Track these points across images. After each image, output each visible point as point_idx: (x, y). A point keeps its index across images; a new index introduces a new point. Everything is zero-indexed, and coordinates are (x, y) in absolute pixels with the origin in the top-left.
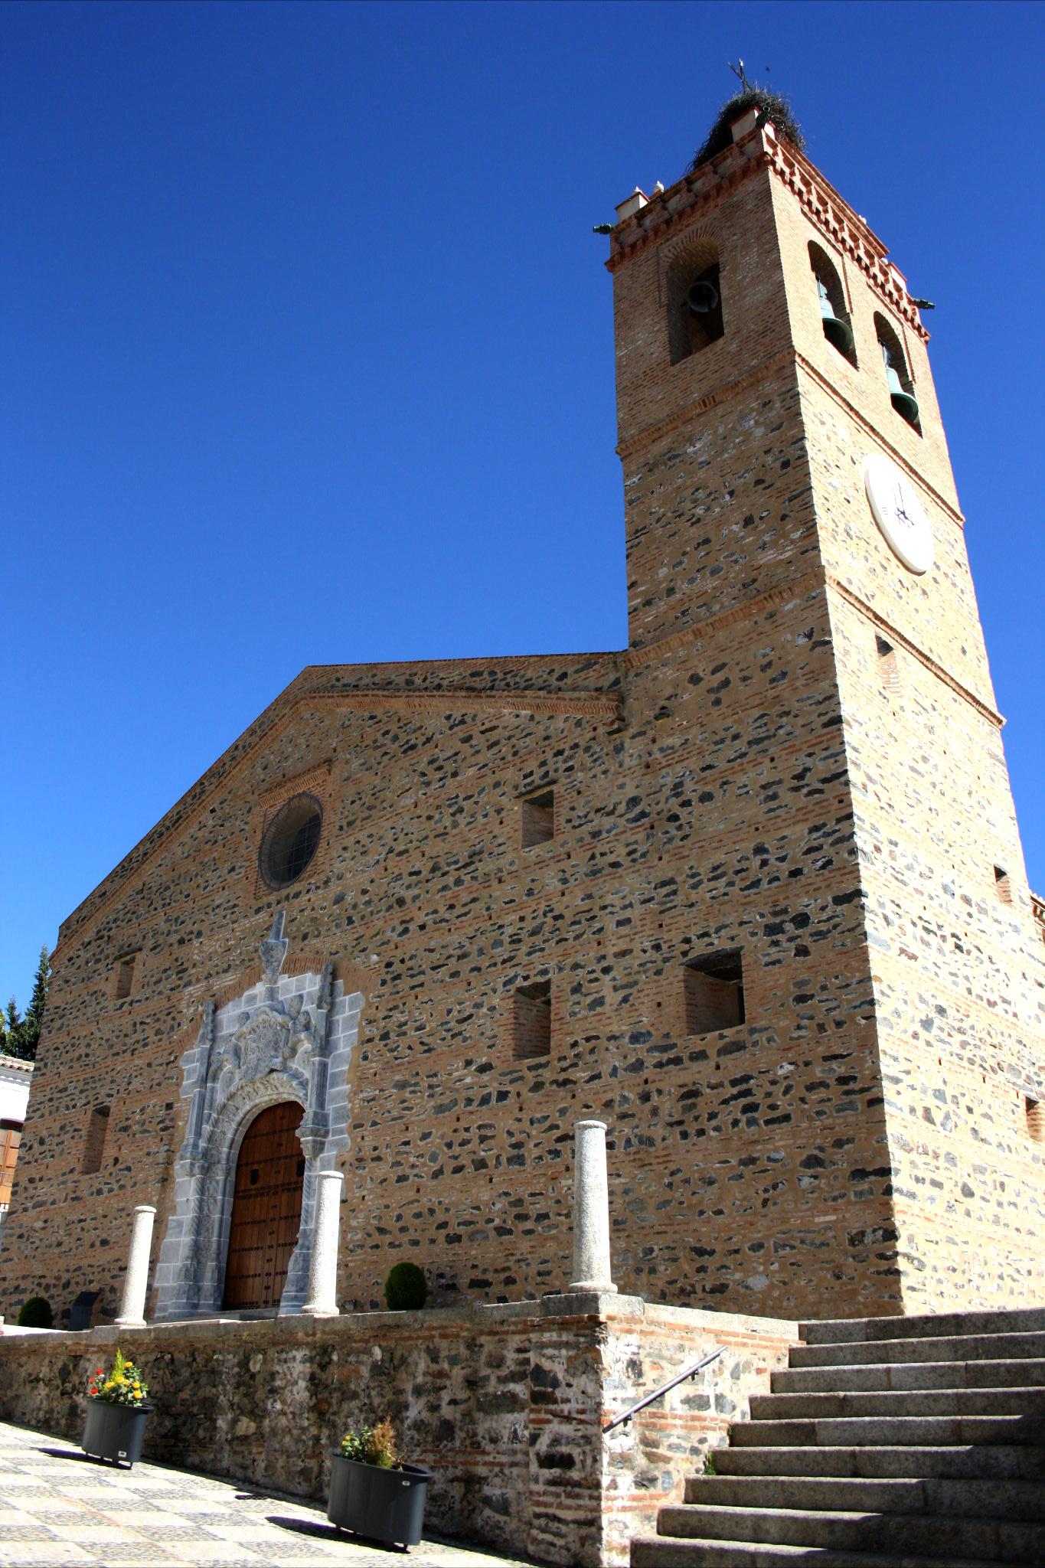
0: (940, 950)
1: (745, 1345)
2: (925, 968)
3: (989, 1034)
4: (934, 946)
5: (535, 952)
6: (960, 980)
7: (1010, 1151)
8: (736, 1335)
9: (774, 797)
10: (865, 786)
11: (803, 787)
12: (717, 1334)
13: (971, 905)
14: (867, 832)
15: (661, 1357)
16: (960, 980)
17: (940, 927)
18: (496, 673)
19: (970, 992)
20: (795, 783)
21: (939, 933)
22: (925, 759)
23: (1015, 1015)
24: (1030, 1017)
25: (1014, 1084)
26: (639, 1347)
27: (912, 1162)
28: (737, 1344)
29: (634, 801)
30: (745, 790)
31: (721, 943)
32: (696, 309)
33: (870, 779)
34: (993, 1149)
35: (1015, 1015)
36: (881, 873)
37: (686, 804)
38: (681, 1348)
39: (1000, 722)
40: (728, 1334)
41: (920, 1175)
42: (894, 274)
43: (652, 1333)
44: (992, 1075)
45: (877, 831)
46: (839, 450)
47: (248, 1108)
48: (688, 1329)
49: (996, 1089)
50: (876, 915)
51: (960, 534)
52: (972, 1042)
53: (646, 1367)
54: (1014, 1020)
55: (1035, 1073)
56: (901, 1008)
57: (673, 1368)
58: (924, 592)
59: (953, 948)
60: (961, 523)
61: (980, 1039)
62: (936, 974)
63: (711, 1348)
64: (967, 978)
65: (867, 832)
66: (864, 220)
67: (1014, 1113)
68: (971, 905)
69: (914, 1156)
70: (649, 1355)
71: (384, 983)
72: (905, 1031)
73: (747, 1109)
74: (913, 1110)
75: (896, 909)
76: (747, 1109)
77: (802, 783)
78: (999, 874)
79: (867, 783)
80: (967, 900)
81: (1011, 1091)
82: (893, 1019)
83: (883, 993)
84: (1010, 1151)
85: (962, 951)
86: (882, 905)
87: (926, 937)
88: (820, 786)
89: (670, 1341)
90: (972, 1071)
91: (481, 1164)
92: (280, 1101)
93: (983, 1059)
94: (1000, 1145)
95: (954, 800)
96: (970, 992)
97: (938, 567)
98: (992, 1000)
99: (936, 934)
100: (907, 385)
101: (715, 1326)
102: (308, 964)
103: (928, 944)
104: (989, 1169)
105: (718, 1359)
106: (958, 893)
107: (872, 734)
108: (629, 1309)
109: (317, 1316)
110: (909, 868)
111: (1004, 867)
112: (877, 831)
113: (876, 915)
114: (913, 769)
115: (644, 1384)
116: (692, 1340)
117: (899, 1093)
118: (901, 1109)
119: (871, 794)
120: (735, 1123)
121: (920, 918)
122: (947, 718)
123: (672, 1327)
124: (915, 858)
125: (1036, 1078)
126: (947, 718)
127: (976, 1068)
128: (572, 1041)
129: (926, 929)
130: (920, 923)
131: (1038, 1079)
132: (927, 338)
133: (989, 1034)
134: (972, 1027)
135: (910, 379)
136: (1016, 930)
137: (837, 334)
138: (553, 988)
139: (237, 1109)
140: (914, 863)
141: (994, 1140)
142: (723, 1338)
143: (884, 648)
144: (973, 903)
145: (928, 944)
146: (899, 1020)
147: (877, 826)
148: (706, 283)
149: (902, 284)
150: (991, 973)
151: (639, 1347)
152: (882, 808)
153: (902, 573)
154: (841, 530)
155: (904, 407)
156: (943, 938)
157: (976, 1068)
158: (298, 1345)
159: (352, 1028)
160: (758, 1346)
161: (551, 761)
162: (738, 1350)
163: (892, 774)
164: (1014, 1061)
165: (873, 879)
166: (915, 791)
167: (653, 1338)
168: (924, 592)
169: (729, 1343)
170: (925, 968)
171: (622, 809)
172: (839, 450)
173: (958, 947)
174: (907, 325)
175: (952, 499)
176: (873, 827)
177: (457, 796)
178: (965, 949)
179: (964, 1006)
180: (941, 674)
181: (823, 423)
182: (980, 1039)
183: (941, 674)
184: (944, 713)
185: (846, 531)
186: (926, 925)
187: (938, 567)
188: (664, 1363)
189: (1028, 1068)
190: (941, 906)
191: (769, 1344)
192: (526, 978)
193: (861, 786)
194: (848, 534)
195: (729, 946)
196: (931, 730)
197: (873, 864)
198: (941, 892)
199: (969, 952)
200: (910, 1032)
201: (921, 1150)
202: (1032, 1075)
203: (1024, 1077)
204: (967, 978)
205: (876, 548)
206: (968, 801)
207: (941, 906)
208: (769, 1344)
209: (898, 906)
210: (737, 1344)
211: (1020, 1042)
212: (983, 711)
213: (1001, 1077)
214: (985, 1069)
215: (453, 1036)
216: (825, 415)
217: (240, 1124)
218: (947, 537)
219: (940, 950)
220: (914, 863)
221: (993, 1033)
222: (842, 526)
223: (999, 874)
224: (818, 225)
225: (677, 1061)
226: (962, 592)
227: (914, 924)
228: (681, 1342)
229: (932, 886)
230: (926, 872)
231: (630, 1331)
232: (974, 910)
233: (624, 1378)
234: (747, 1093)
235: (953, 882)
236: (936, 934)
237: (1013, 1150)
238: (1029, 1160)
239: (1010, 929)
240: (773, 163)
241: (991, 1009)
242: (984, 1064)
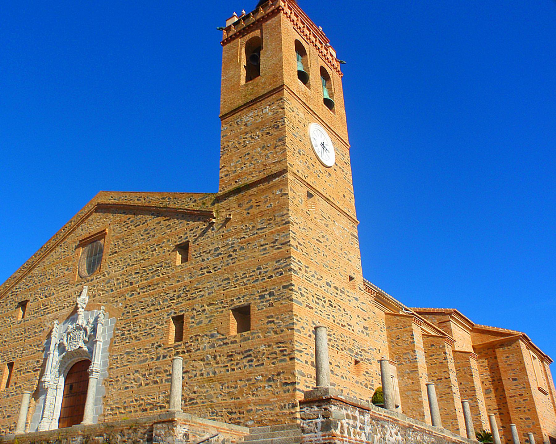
0: (323, 306)
1: (228, 433)
2: (316, 312)
3: (341, 337)
4: (321, 305)
5: (179, 303)
6: (331, 317)
7: (346, 379)
8: (224, 429)
9: (265, 249)
10: (297, 246)
11: (275, 246)
12: (217, 428)
13: (338, 290)
14: (296, 263)
15: (196, 434)
16: (331, 317)
17: (324, 298)
18: (171, 199)
19: (334, 321)
20: (272, 245)
21: (323, 300)
22: (323, 237)
23: (353, 330)
24: (359, 331)
25: (350, 355)
26: (188, 430)
27: (305, 380)
28: (224, 432)
29: (216, 249)
30: (255, 246)
31: (243, 303)
32: (252, 63)
33: (299, 243)
34: (340, 378)
35: (353, 330)
36: (301, 278)
37: (235, 250)
38: (204, 432)
39: (357, 222)
40: (221, 429)
41: (308, 385)
42: (331, 50)
43: (193, 426)
44: (341, 351)
45: (300, 263)
46: (299, 121)
47: (70, 362)
48: (207, 425)
49: (342, 356)
50: (298, 293)
51: (348, 152)
52: (334, 339)
53: (190, 436)
54: (353, 332)
55: (360, 351)
56: (305, 326)
57: (200, 438)
58: (329, 174)
59: (329, 305)
60: (348, 148)
61: (337, 338)
62: (321, 315)
63: (215, 433)
64: (333, 316)
65: (296, 263)
66: (321, 29)
67: (349, 365)
68: (338, 290)
69: (306, 378)
70: (192, 432)
71: (123, 314)
72: (306, 334)
73: (249, 361)
74: (306, 362)
75: (306, 291)
76: (249, 361)
77: (274, 245)
78: (351, 278)
79: (298, 245)
80: (336, 288)
81: (349, 357)
82: (302, 330)
83: (297, 320)
84: (346, 379)
85: (332, 307)
86: (300, 289)
87: (317, 301)
88: (280, 246)
89: (199, 429)
90: (333, 349)
91: (156, 382)
92: (83, 359)
93: (338, 345)
94: (342, 376)
95: (334, 252)
96: (334, 321)
97: (337, 165)
98: (343, 324)
99: (321, 300)
100: (331, 95)
101: (217, 426)
102: (95, 307)
103: (318, 304)
104: (337, 385)
105: (217, 436)
106: (333, 285)
107: (302, 227)
108: (186, 418)
109: (85, 425)
110: (313, 276)
111: (353, 276)
112: (300, 263)
113: (298, 293)
114: (317, 240)
115: (189, 442)
116: (208, 429)
117: (301, 356)
118: (302, 362)
119: (299, 249)
120: (245, 366)
121: (316, 294)
122: (334, 221)
123: (201, 424)
124: (315, 273)
125: (360, 353)
126: (334, 221)
127: (334, 349)
128: (190, 336)
129: (318, 299)
130: (315, 296)
131: (361, 354)
132: (342, 75)
133: (341, 337)
134: (334, 334)
135: (333, 92)
136: (356, 299)
137: (303, 77)
138: (185, 316)
139: (65, 362)
140: (315, 274)
141: (340, 375)
142: (219, 430)
143: (310, 195)
144: (339, 289)
145: (318, 304)
146: (304, 330)
147: (300, 260)
148: (256, 54)
149: (334, 54)
150: (344, 315)
151: (188, 430)
152: (303, 254)
153: (321, 167)
154: (296, 152)
155: (329, 103)
156: (325, 302)
157: (334, 349)
158: (79, 435)
159: (111, 331)
160: (233, 434)
161: (188, 232)
162: (224, 434)
163: (309, 242)
164: (351, 347)
165: (297, 280)
166: (318, 248)
167: (193, 427)
168: (329, 174)
169: (222, 432)
170: (316, 312)
171: (212, 252)
172: (299, 121)
173: (330, 305)
174: (334, 70)
175: (346, 138)
176: (299, 261)
177: (154, 244)
178: (333, 306)
179: (331, 326)
180: (332, 205)
181: (293, 111)
182: (337, 338)
183: (332, 205)
184: (333, 219)
185: (298, 152)
186: (318, 297)
187: (337, 165)
188: (197, 436)
189: (357, 350)
190: (325, 290)
191: (237, 434)
192: (175, 313)
193: (295, 246)
194: (299, 153)
195: (246, 303)
196: (327, 226)
197: (298, 274)
198: (325, 285)
199: (335, 307)
200: (308, 335)
201: (309, 376)
202: (358, 352)
203: (355, 353)
204: (333, 316)
205: (311, 158)
206: (340, 252)
207: (325, 290)
208: (237, 434)
209: (307, 290)
210: (224, 432)
211: (354, 340)
212: (350, 219)
213: (345, 352)
214: (338, 349)
215: (148, 334)
216: (295, 108)
217: (66, 368)
218: (342, 153)
219: (323, 306)
220: (315, 274)
221: (343, 336)
222: (297, 151)
223: (351, 278)
224: (300, 33)
225: (226, 344)
226: (346, 174)
227: (313, 296)
228: (204, 430)
229: (322, 283)
230: (320, 277)
231: (185, 424)
232: (339, 292)
233: (182, 439)
234: (250, 355)
235: (331, 281)
236: (321, 300)
237: (348, 379)
238: (354, 382)
239: (354, 299)
240: (283, 9)
241: (342, 328)
242: (338, 347)
